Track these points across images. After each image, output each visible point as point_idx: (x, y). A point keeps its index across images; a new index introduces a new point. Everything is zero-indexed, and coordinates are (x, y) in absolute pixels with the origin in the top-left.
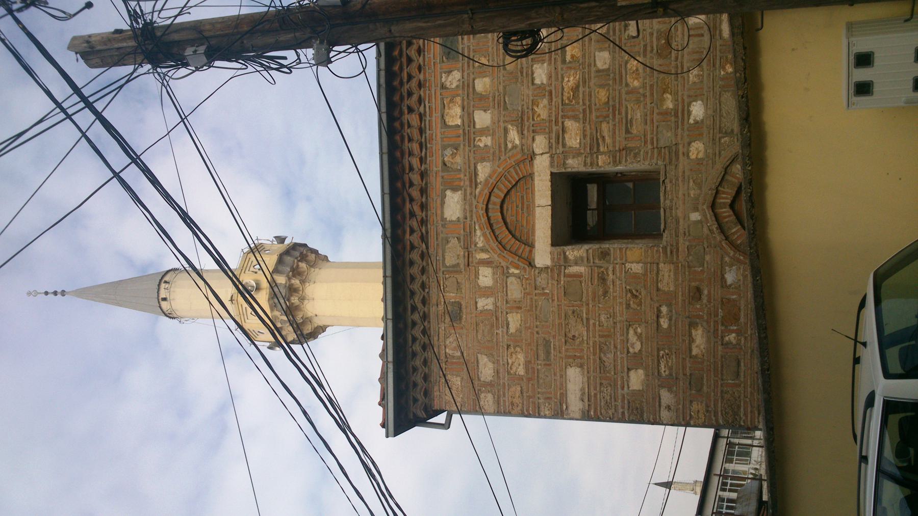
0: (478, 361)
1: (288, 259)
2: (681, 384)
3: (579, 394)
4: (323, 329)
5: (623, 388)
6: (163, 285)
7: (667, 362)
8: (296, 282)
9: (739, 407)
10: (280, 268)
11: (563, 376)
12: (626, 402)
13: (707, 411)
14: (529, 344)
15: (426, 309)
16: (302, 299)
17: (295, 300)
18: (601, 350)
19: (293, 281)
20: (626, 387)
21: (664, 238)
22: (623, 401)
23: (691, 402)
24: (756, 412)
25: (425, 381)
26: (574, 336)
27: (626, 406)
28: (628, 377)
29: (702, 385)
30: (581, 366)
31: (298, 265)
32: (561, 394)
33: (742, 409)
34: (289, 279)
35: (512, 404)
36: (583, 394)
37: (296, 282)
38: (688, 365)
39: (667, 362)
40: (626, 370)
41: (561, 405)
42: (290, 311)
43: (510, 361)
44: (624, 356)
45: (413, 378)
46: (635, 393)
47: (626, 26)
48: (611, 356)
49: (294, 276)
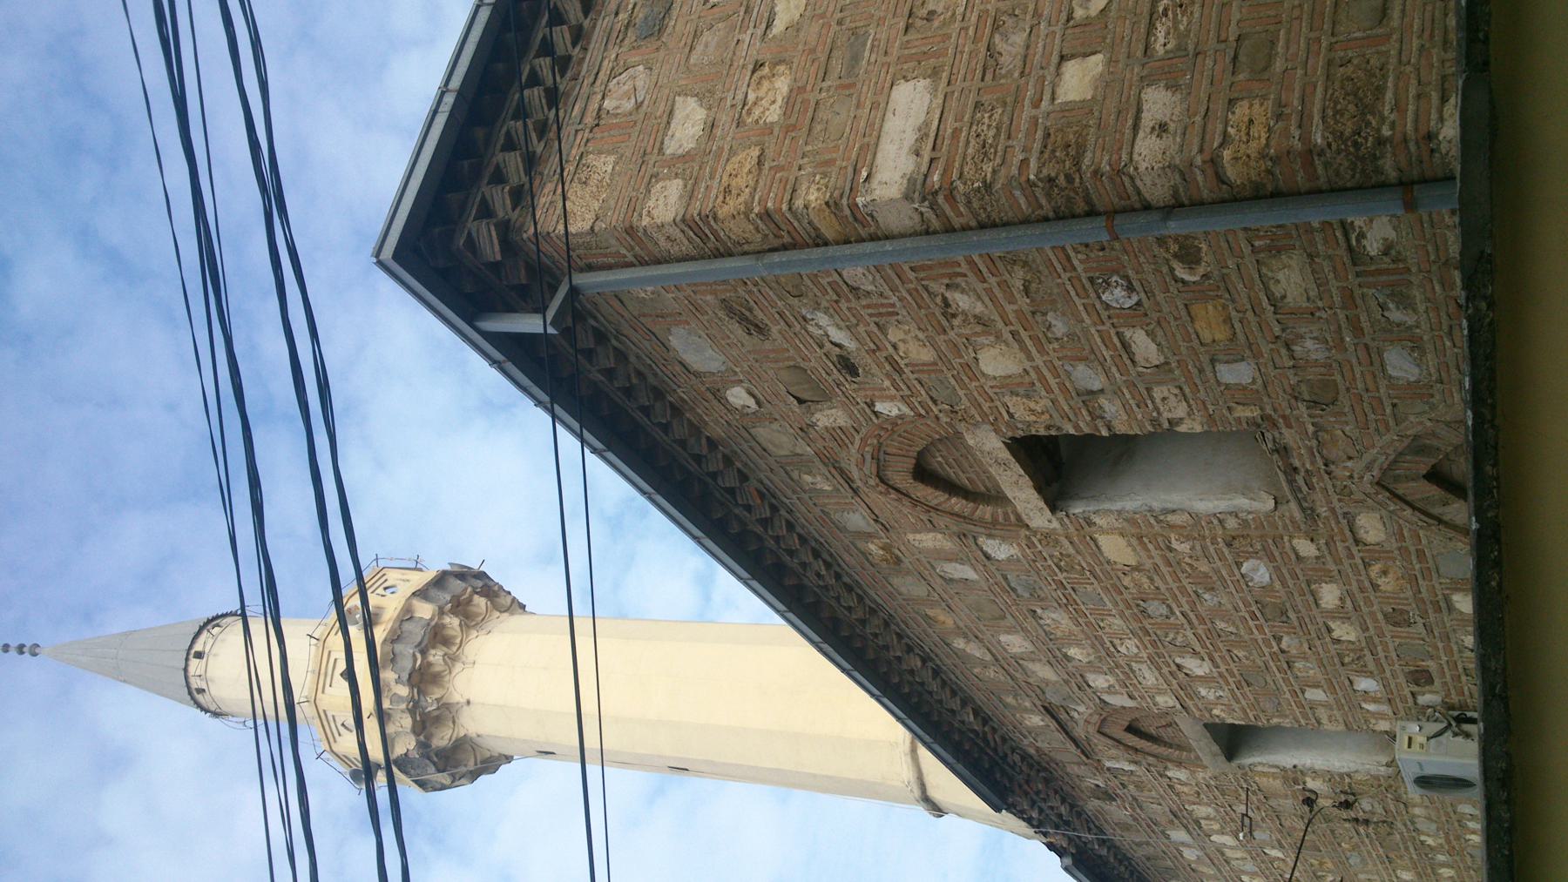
0: (671, 113)
1: (457, 585)
2: (1209, 62)
3: (910, 137)
4: (490, 764)
5: (1036, 105)
6: (194, 662)
7: (1176, 22)
8: (452, 622)
9: (1380, 91)
10: (433, 592)
11: (880, 106)
12: (1039, 134)
13: (1279, 117)
14: (813, 51)
15: (586, 23)
16: (452, 659)
17: (436, 656)
18: (996, 27)
19: (447, 620)
20: (1047, 97)
21: (1402, 679)
22: (1030, 133)
23: (1231, 102)
24: (1435, 97)
25: (528, 171)
26: (932, 13)
27: (1037, 146)
28: (1058, 74)
29: (1270, 58)
30: (935, 74)
31: (470, 601)
32: (864, 148)
33: (1389, 95)
34: (441, 612)
35: (727, 191)
36: (922, 139)
37: (452, 622)
38: (1236, 16)
39: (1176, 22)
40: (1055, 59)
41: (856, 171)
42: (423, 679)
43: (751, 97)
44: (1058, 29)
45: (499, 157)
46: (1069, 108)
47: (1458, 720)
48: (1019, 39)
49: (454, 612)
